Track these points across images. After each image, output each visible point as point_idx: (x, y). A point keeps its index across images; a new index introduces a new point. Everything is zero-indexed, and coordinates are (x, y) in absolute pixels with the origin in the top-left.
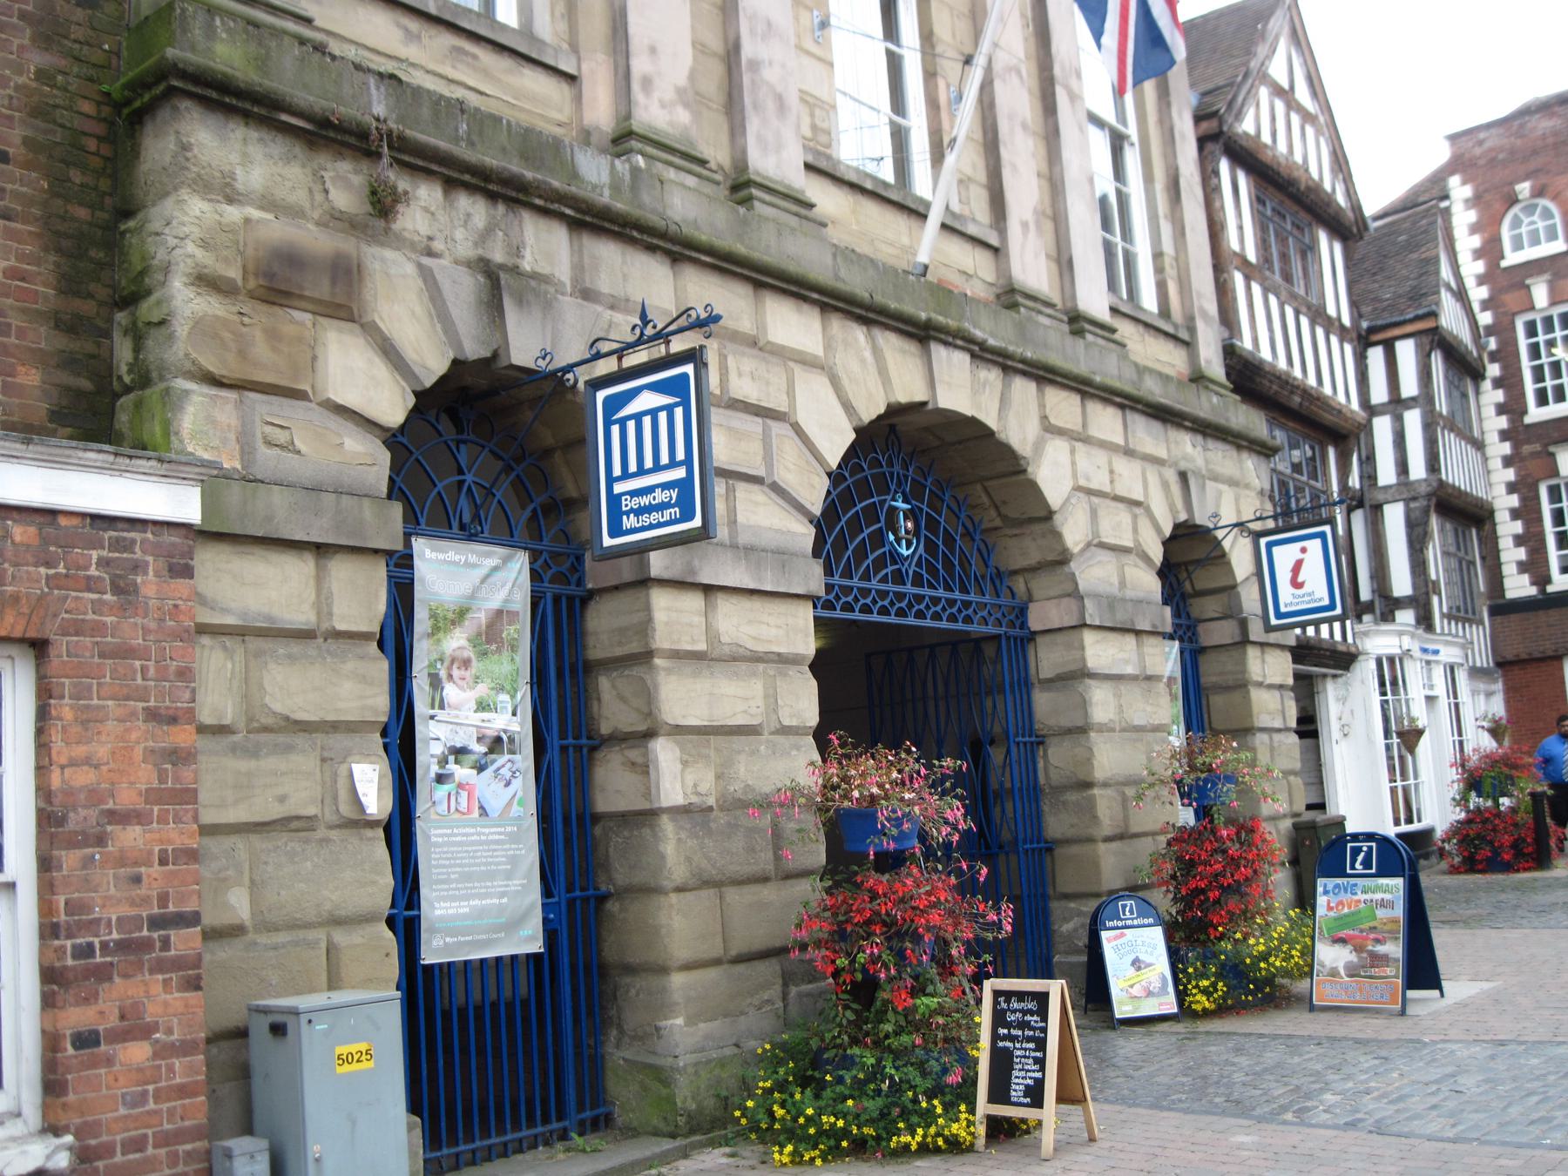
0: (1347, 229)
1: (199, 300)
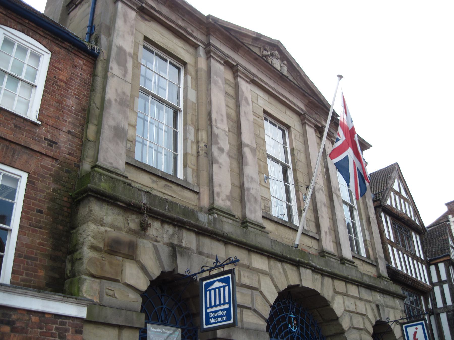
0: (420, 230)
1: (91, 253)
